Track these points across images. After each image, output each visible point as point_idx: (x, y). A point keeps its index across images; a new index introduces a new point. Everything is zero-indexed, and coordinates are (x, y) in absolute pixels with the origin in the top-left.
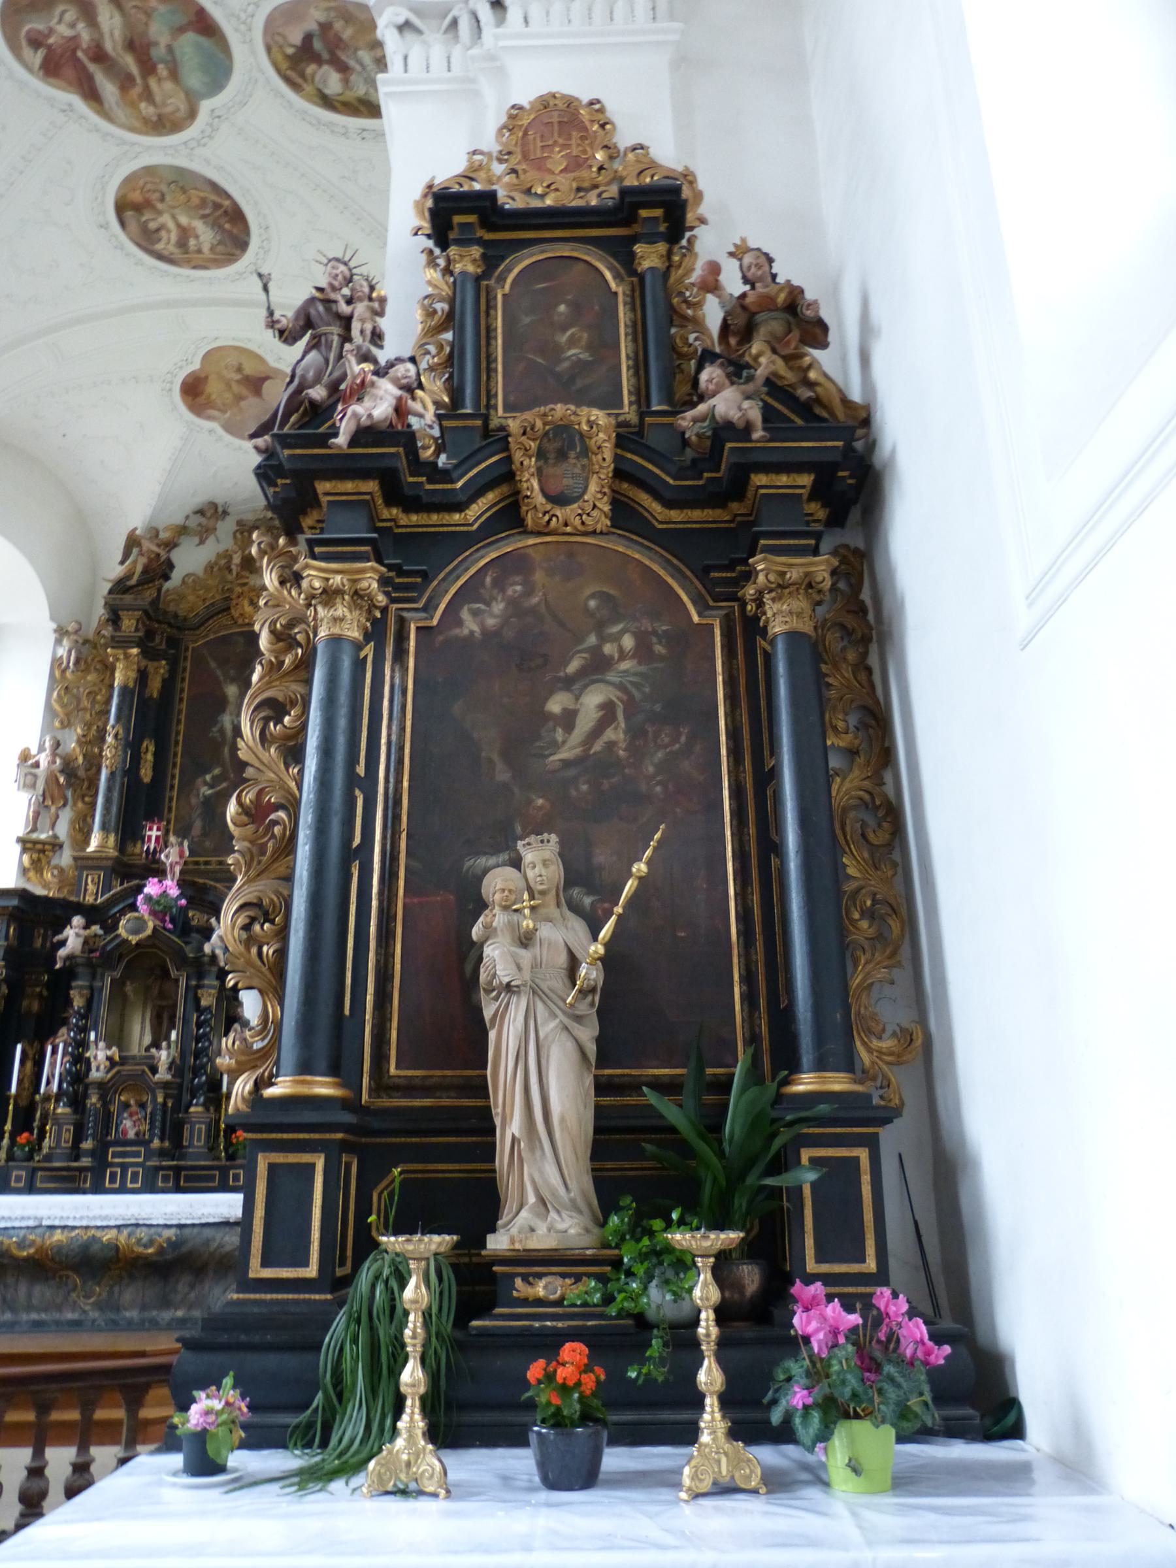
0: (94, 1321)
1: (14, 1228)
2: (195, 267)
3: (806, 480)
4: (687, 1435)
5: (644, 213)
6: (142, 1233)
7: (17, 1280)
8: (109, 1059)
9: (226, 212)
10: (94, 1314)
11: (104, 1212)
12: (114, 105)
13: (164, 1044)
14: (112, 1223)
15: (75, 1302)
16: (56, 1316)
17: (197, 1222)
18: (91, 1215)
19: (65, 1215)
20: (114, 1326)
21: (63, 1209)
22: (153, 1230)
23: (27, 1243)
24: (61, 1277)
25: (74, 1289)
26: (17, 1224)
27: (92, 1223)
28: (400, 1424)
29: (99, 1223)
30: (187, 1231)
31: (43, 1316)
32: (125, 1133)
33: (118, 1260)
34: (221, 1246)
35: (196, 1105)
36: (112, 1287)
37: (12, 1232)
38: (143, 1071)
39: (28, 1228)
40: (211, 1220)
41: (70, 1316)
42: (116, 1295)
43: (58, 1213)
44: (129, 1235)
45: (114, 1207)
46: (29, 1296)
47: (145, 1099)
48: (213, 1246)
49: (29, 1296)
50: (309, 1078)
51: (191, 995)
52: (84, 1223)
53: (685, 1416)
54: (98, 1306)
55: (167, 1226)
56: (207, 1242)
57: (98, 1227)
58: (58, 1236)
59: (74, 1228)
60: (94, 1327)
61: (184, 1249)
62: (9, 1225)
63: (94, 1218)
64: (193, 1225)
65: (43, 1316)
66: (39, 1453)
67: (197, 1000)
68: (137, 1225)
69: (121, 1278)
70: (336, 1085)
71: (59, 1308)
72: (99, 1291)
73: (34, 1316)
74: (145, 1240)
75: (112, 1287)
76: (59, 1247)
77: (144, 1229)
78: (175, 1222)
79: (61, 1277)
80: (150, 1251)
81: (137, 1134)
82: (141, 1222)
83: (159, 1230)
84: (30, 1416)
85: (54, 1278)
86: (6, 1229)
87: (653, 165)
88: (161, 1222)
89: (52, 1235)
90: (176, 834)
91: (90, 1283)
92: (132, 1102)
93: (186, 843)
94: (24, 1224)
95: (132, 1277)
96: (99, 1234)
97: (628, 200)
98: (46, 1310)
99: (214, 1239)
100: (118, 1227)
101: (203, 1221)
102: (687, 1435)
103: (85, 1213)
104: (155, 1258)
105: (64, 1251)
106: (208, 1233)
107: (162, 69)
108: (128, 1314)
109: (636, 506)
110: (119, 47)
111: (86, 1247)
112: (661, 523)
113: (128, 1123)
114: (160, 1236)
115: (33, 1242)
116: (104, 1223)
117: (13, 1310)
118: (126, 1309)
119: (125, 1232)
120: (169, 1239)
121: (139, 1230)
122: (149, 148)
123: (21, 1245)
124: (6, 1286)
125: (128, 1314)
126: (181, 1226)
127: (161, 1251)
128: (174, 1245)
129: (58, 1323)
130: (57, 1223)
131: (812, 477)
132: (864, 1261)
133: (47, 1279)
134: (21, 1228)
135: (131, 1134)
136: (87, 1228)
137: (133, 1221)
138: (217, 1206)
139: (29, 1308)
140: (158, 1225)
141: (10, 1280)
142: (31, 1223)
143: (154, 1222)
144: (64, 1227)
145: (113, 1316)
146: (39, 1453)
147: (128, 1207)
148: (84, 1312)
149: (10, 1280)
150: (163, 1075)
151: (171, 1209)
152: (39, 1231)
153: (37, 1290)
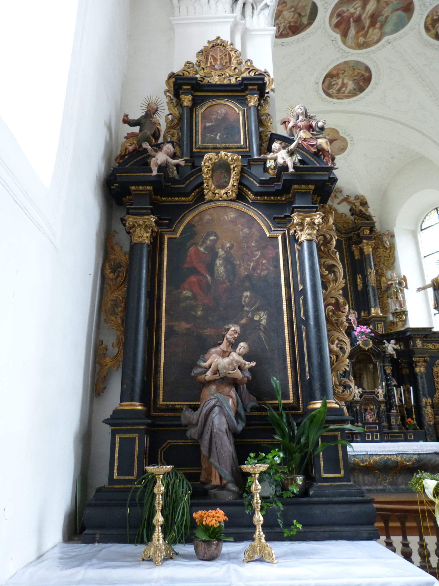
0: (390, 489)
1: (358, 455)
2: (338, 99)
3: (312, 187)
4: (249, 537)
5: (251, 87)
6: (405, 457)
7: (358, 475)
8: (359, 392)
9: (364, 78)
10: (389, 487)
11: (391, 449)
12: (350, 38)
13: (380, 387)
14: (394, 453)
15: (381, 483)
16: (375, 487)
17: (425, 453)
18: (386, 450)
19: (376, 450)
20: (397, 491)
21: (417, 447)
22: (409, 456)
23: (364, 460)
24: (374, 473)
25: (379, 478)
26: (359, 454)
27: (387, 453)
28: (328, 530)
29: (389, 453)
30: (422, 456)
31: (370, 487)
32: (368, 420)
33: (397, 466)
34: (435, 462)
35: (393, 410)
36: (393, 477)
37: (358, 456)
38: (374, 397)
39: (363, 455)
40: (430, 452)
41: (380, 487)
42: (395, 480)
43: (373, 449)
44: (401, 457)
45: (389, 447)
46: (364, 480)
47: (372, 407)
48: (433, 461)
49: (364, 480)
50: (133, 403)
51: (382, 368)
52: (384, 453)
53: (250, 530)
54: (390, 484)
55: (414, 454)
56: (430, 460)
57: (388, 455)
58: (377, 458)
59: (380, 455)
60: (390, 492)
61: (422, 463)
62: (356, 454)
63: (387, 451)
64: (424, 454)
65: (370, 487)
66: (405, 538)
67: (385, 371)
68: (403, 454)
69: (396, 473)
70: (141, 405)
71: (376, 484)
72: (389, 479)
73: (367, 487)
74: (407, 459)
75: (393, 477)
76: (375, 461)
77: (405, 455)
78: (417, 453)
79: (374, 473)
80: (410, 463)
81: (373, 420)
82: (404, 453)
83: (411, 455)
84: (398, 524)
85: (371, 473)
86: (355, 455)
87: (254, 70)
88: (412, 453)
89: (372, 457)
90: (353, 309)
91: (385, 476)
92: (369, 409)
93: (356, 313)
94: (361, 454)
95: (400, 473)
96: (389, 457)
97: (244, 82)
98: (371, 485)
99: (433, 459)
100: (396, 454)
101: (428, 452)
102: (249, 537)
103: (384, 450)
104: (410, 466)
105: (378, 464)
106: (429, 456)
107: (378, 25)
108: (401, 487)
109: (244, 194)
110: (367, 17)
111: (386, 462)
112: (191, 201)
113: (368, 416)
114: (412, 457)
115: (366, 460)
116: (391, 453)
117: (360, 486)
118: (400, 485)
119: (400, 456)
120: (416, 459)
121: (404, 455)
122: (352, 54)
123: (362, 461)
124: (354, 476)
125: (401, 487)
126: (419, 454)
127: (414, 463)
128: (418, 461)
129: (376, 490)
130: (374, 453)
131: (314, 186)
132: (325, 473)
133: (369, 474)
134: (361, 455)
135: (371, 420)
136: (385, 455)
137: (402, 452)
138: (431, 447)
139: (365, 485)
140: (411, 454)
141: (356, 474)
142: (364, 453)
143: (410, 453)
144: (376, 455)
145: (395, 487)
146: (405, 538)
147: (398, 447)
148: (385, 486)
149: (356, 474)
150: (381, 398)
151: (415, 448)
152: (367, 456)
153: (366, 478)
